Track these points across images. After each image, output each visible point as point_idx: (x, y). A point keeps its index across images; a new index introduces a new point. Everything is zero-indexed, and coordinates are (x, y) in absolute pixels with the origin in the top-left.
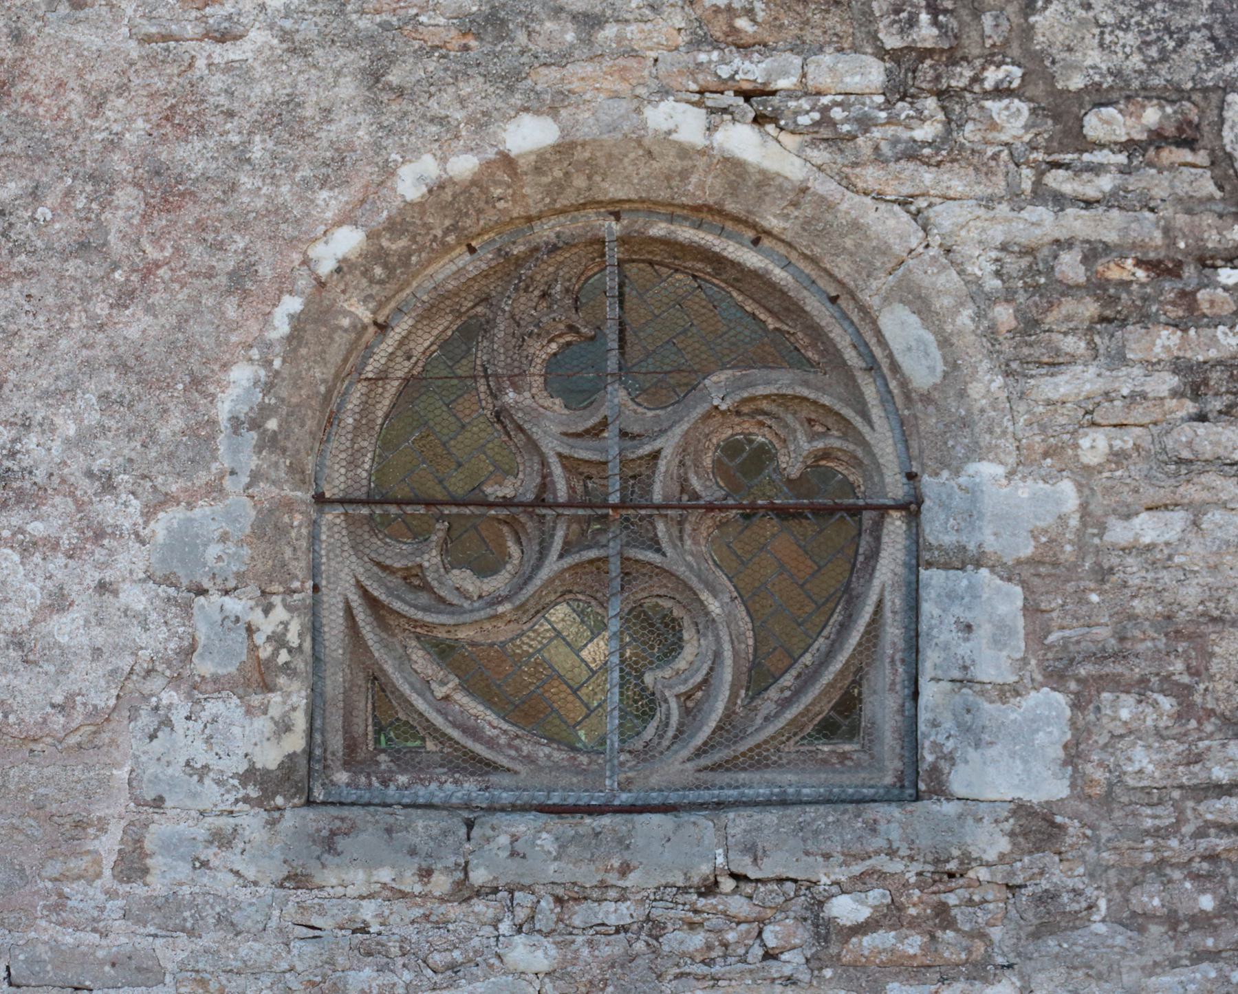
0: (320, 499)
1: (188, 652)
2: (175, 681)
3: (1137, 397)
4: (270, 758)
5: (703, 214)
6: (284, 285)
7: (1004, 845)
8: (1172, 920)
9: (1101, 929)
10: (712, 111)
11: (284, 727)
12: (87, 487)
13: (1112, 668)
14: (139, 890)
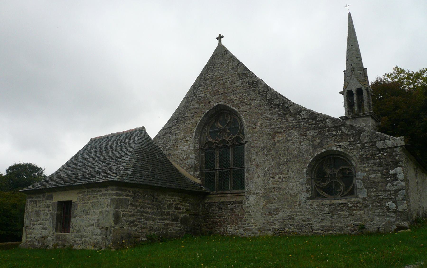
0: (312, 178)
1: (303, 189)
2: (302, 191)
3: (371, 166)
4: (309, 196)
5: (338, 155)
6: (307, 163)
7: (362, 200)
8: (376, 206)
10: (337, 147)
11: (310, 195)
12: (295, 178)
13: (139, 151)
14: (300, 206)
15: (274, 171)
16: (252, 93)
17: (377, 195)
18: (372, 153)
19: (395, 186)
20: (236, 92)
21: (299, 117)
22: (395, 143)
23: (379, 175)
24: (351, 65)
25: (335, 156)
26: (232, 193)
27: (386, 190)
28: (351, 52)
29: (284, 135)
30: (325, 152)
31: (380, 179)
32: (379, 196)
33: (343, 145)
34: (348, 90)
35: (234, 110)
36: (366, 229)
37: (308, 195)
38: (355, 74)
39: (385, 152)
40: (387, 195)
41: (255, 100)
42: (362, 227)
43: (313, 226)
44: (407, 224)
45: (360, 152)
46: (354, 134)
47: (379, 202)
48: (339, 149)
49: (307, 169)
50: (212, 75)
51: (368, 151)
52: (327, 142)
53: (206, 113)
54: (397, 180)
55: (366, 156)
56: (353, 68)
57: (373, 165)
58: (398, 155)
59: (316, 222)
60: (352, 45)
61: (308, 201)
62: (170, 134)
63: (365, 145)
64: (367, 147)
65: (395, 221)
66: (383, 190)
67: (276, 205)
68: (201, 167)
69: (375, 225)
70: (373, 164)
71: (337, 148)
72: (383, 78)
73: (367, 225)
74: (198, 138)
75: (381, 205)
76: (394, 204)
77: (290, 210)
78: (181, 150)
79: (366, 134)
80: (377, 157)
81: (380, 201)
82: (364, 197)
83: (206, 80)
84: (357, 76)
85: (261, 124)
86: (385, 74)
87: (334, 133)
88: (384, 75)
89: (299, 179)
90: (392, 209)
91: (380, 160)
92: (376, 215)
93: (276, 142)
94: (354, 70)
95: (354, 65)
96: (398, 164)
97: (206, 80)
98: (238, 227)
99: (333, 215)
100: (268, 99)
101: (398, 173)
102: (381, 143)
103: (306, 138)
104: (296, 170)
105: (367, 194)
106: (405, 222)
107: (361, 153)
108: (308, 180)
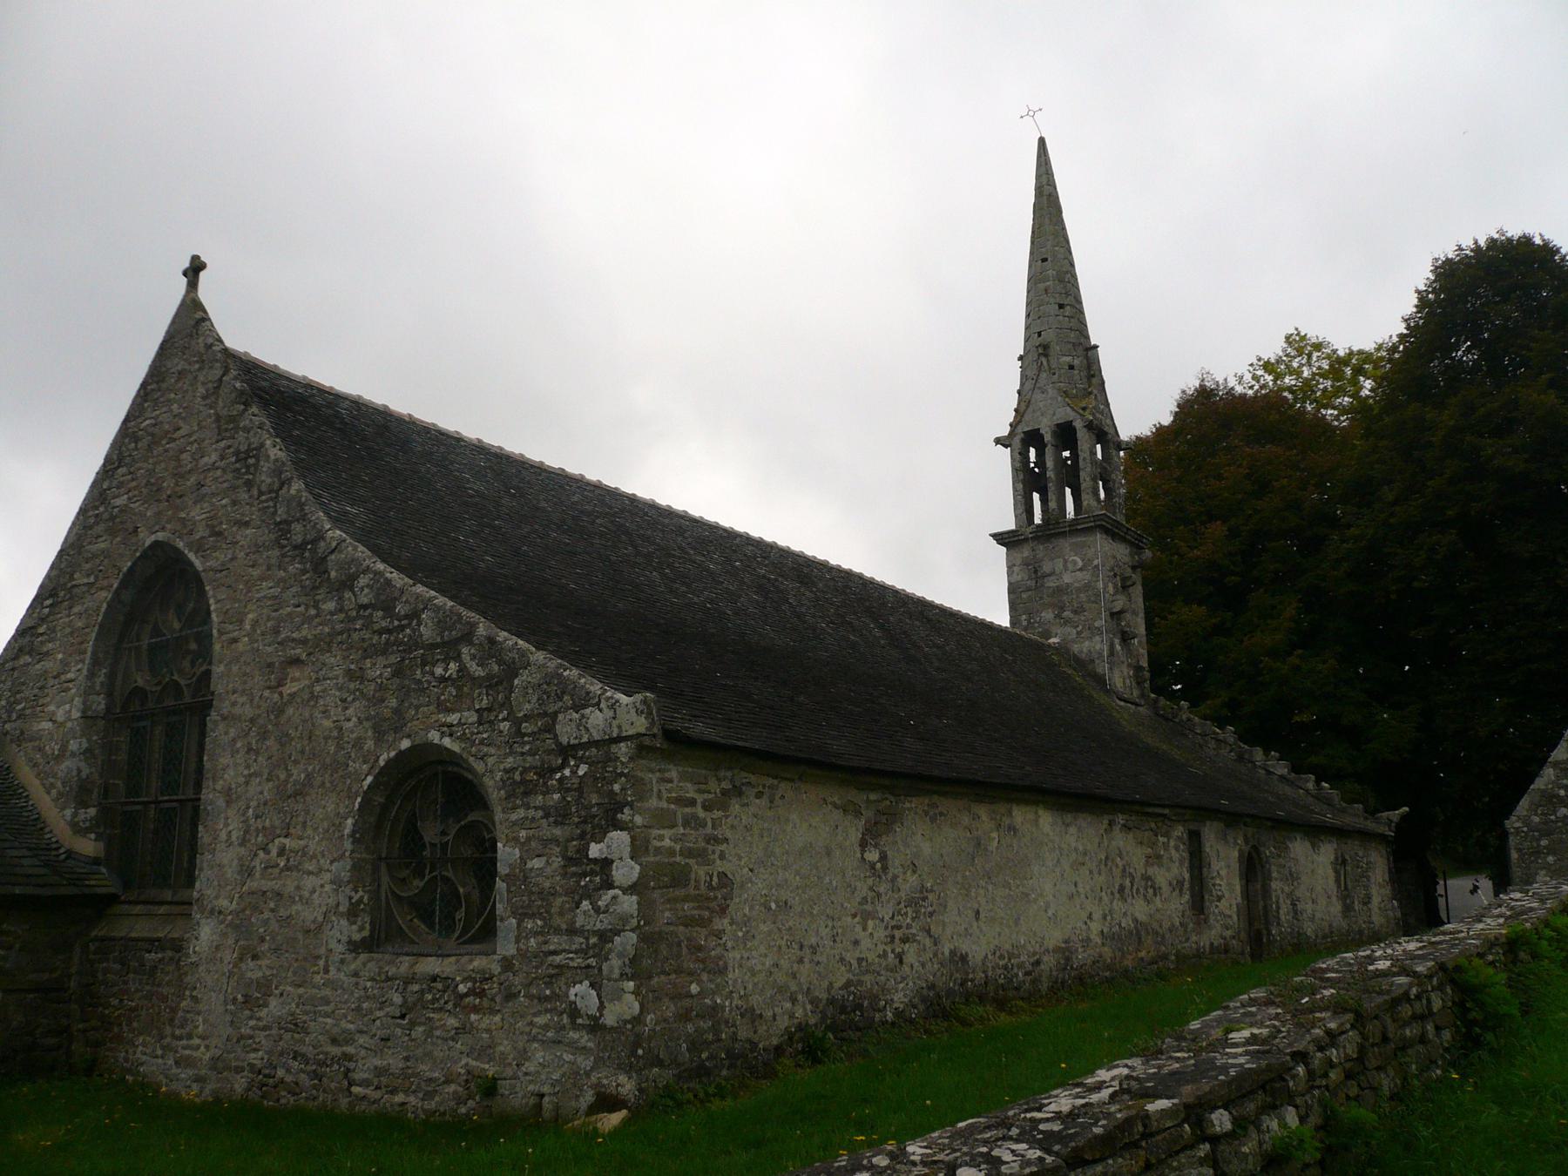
1: (338, 905)
4: (357, 937)
8: (539, 999)
9: (522, 999)
10: (443, 733)
11: (361, 929)
15: (267, 823)
16: (243, 496)
17: (545, 948)
18: (543, 762)
19: (604, 913)
20: (204, 490)
21: (350, 599)
22: (615, 723)
23: (557, 862)
24: (1039, 334)
25: (450, 769)
26: (177, 903)
27: (572, 931)
28: (1042, 286)
29: (308, 670)
30: (408, 750)
31: (558, 878)
32: (555, 953)
33: (460, 724)
34: (1026, 429)
35: (191, 564)
36: (502, 1095)
37: (356, 931)
38: (1050, 368)
39: (581, 760)
40: (576, 952)
41: (247, 524)
42: (490, 1088)
43: (352, 1065)
44: (628, 1087)
45: (506, 756)
46: (493, 677)
47: (550, 980)
48: (447, 742)
49: (356, 821)
50: (153, 421)
51: (532, 753)
52: (417, 708)
53: (124, 574)
54: (611, 886)
55: (521, 774)
56: (1046, 347)
57: (542, 818)
58: (622, 774)
59: (366, 1048)
60: (1044, 260)
61: (349, 957)
62: (30, 653)
63: (524, 725)
64: (529, 735)
65: (592, 1069)
66: (564, 926)
67: (264, 962)
68: (106, 791)
69: (531, 1082)
70: (540, 813)
71: (443, 734)
72: (1251, 375)
73: (505, 1079)
74: (104, 671)
75: (555, 996)
76: (594, 993)
77: (301, 991)
78: (51, 720)
79: (529, 679)
80: (554, 782)
81: (551, 976)
82: (507, 954)
83: (136, 443)
84: (1056, 376)
85: (255, 623)
86: (1255, 362)
87: (439, 671)
88: (1251, 365)
89: (332, 862)
90: (585, 1017)
91: (564, 798)
92: (534, 1039)
93: (286, 698)
94: (1046, 356)
95: (1048, 336)
96: (619, 816)
97: (136, 443)
98: (163, 1048)
99: (413, 1024)
100: (280, 523)
101: (615, 856)
102: (571, 720)
103: (362, 687)
104: (326, 824)
105: (517, 942)
106: (623, 1078)
107: (510, 762)
108: (356, 867)
